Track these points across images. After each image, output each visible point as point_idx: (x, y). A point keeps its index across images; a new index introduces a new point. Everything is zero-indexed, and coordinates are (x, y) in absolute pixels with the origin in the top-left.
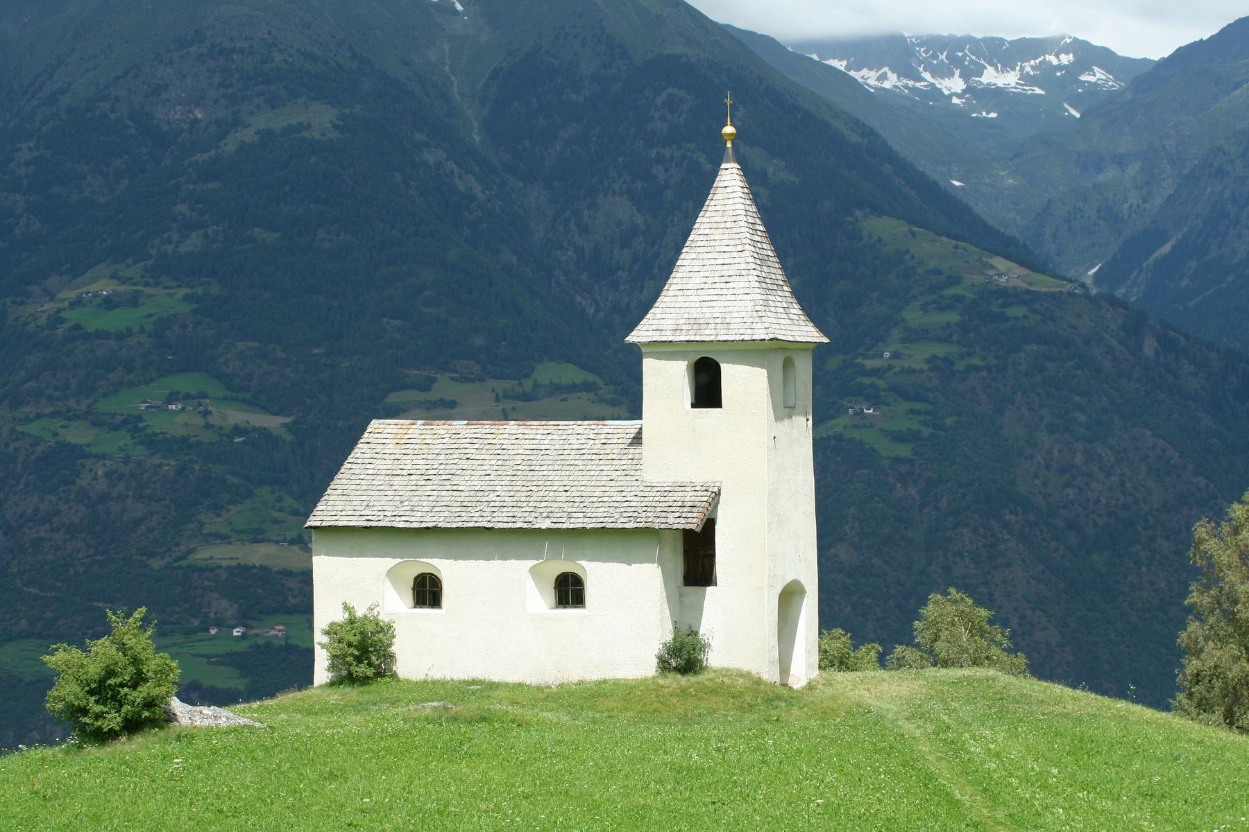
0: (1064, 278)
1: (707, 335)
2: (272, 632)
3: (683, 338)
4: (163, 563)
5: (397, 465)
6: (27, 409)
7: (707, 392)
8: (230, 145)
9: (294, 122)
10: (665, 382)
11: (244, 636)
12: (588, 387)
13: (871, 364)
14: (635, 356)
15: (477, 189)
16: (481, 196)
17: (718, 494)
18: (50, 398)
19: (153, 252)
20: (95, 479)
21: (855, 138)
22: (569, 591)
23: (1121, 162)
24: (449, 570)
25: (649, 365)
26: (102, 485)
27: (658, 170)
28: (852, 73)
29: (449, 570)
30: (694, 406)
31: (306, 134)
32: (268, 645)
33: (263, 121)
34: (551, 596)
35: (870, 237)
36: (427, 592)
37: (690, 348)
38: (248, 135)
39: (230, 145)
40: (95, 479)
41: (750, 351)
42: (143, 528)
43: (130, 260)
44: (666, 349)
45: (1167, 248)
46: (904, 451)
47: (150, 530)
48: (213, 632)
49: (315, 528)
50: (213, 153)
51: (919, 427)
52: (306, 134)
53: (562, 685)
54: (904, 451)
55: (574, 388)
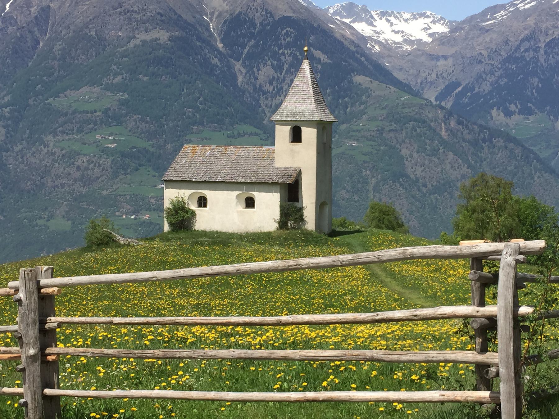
0: (424, 98)
1: (298, 118)
2: (145, 217)
3: (289, 119)
4: (107, 193)
5: (194, 157)
6: (60, 138)
7: (296, 136)
8: (131, 45)
9: (154, 37)
10: (283, 133)
11: (135, 219)
12: (256, 134)
13: (355, 128)
14: (274, 123)
15: (219, 64)
16: (220, 66)
17: (300, 171)
18: (67, 134)
19: (104, 83)
20: (83, 162)
21: (352, 48)
22: (250, 203)
23: (445, 58)
24: (209, 194)
25: (277, 127)
26: (85, 164)
27: (282, 58)
28: (352, 24)
29: (209, 194)
30: (301, 142)
31: (158, 42)
32: (144, 222)
33: (143, 36)
34: (244, 204)
35: (356, 83)
36: (202, 202)
37: (290, 123)
38: (138, 42)
39: (131, 45)
40: (83, 162)
41: (310, 123)
42: (100, 180)
43: (95, 86)
44: (283, 123)
45: (460, 89)
46: (367, 158)
47: (103, 181)
48: (124, 217)
49: (165, 180)
50: (125, 48)
51: (372, 150)
52: (158, 42)
53: (247, 233)
54: (367, 158)
55: (251, 134)
